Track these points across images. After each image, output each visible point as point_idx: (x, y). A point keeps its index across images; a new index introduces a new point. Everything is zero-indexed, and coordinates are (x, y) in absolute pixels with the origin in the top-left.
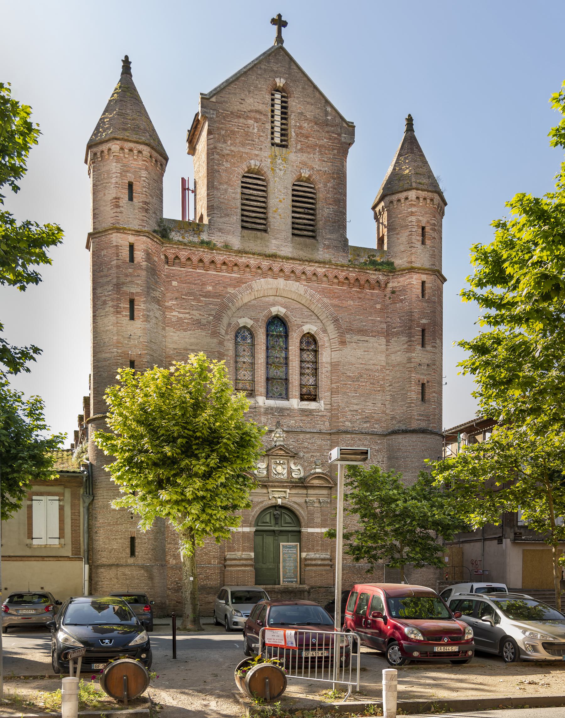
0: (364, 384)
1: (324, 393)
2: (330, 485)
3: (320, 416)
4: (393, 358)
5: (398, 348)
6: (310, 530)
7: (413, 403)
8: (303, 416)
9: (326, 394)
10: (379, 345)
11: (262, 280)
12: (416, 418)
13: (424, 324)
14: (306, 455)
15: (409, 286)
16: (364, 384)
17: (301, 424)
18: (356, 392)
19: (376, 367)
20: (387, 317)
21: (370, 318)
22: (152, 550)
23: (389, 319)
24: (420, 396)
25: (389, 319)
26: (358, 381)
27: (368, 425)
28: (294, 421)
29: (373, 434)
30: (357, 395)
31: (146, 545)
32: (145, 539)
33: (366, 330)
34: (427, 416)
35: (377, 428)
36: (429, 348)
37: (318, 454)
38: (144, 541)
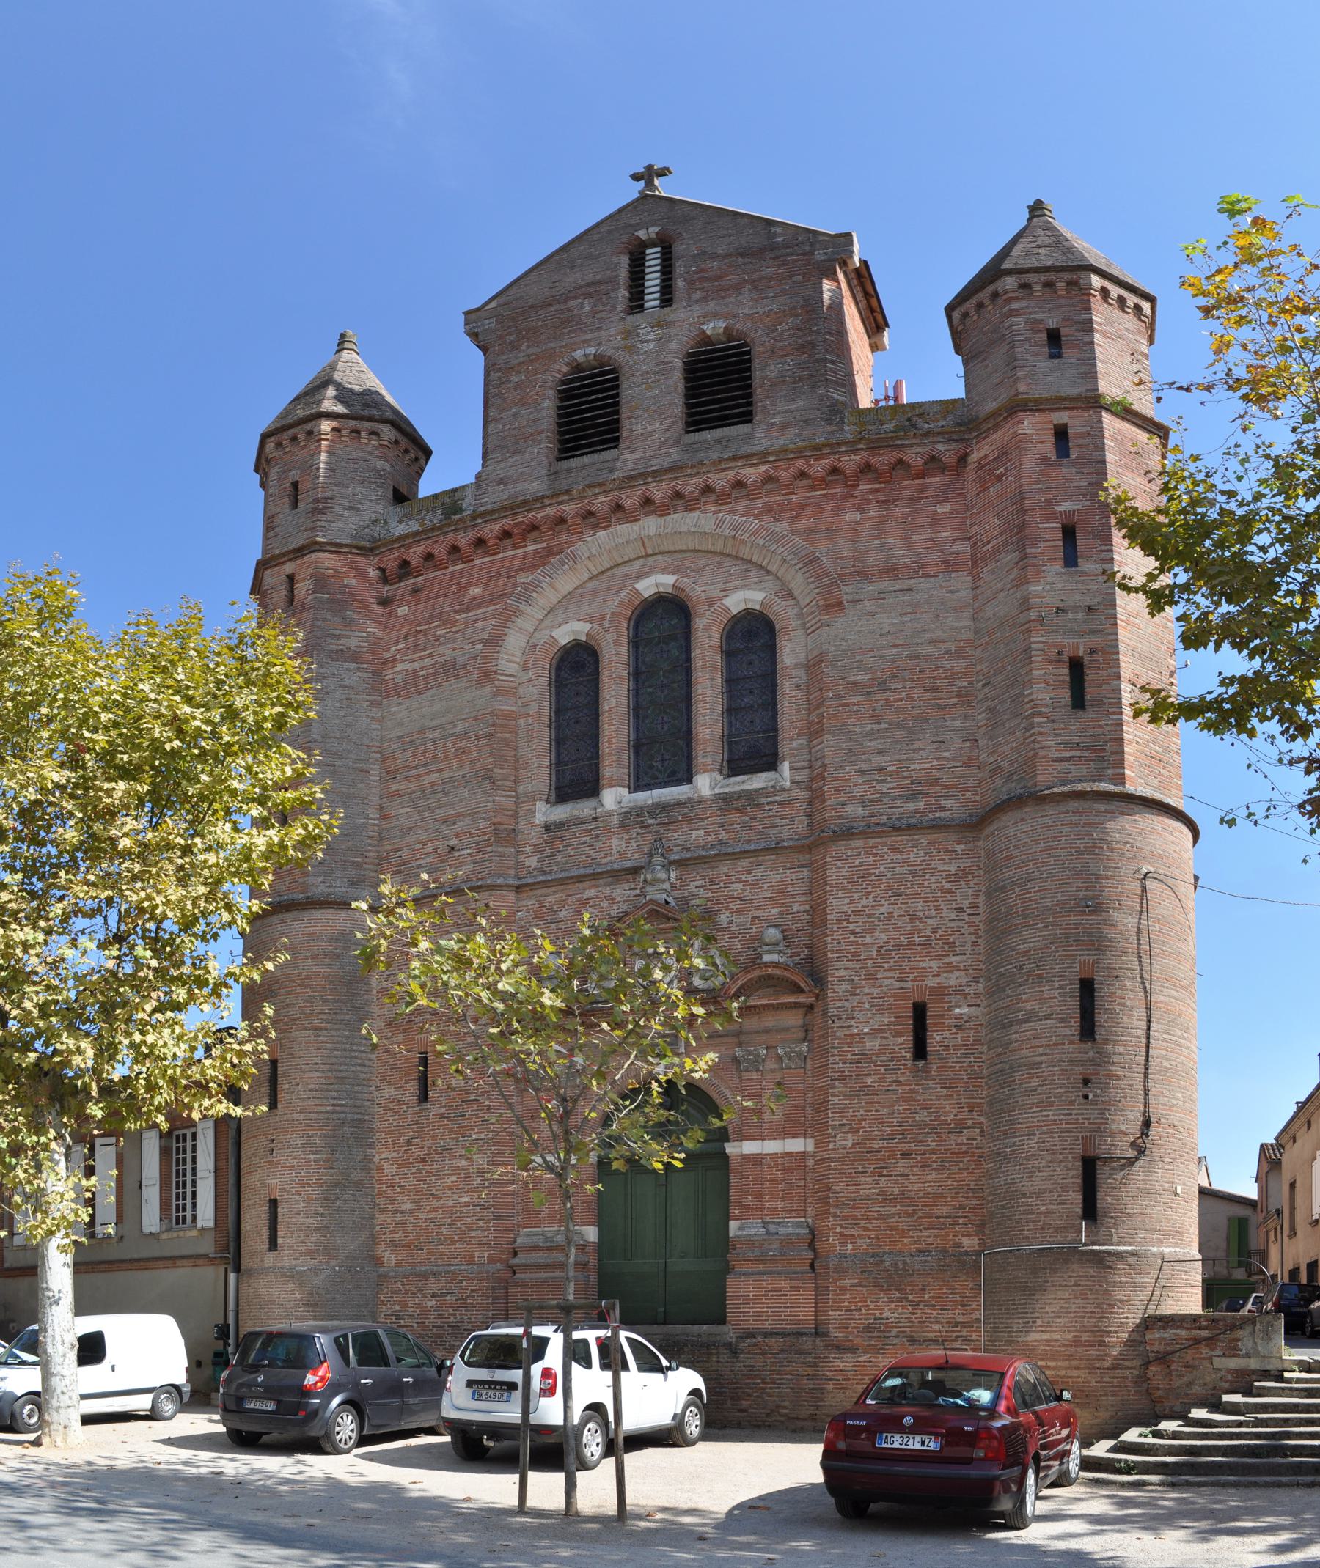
0: (904, 695)
1: (791, 742)
2: (802, 999)
3: (779, 803)
4: (989, 613)
5: (1000, 585)
6: (750, 1147)
7: (1040, 714)
8: (728, 811)
9: (795, 744)
10: (952, 592)
11: (601, 534)
12: (1055, 754)
13: (1070, 514)
14: (737, 920)
15: (1014, 441)
16: (904, 695)
17: (723, 836)
18: (877, 718)
19: (943, 646)
20: (973, 525)
21: (915, 537)
22: (318, 1229)
23: (975, 529)
24: (1066, 694)
25: (975, 529)
26: (884, 691)
27: (921, 804)
28: (702, 832)
29: (935, 826)
30: (883, 726)
31: (301, 1218)
32: (297, 1202)
33: (908, 567)
34: (1093, 748)
35: (952, 808)
36: (1086, 565)
37: (775, 911)
38: (296, 1208)
